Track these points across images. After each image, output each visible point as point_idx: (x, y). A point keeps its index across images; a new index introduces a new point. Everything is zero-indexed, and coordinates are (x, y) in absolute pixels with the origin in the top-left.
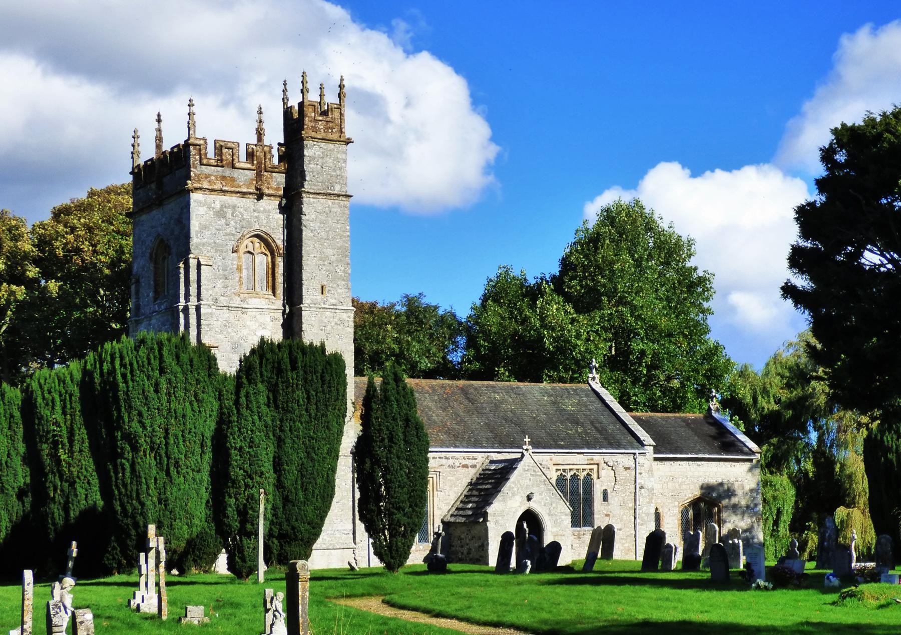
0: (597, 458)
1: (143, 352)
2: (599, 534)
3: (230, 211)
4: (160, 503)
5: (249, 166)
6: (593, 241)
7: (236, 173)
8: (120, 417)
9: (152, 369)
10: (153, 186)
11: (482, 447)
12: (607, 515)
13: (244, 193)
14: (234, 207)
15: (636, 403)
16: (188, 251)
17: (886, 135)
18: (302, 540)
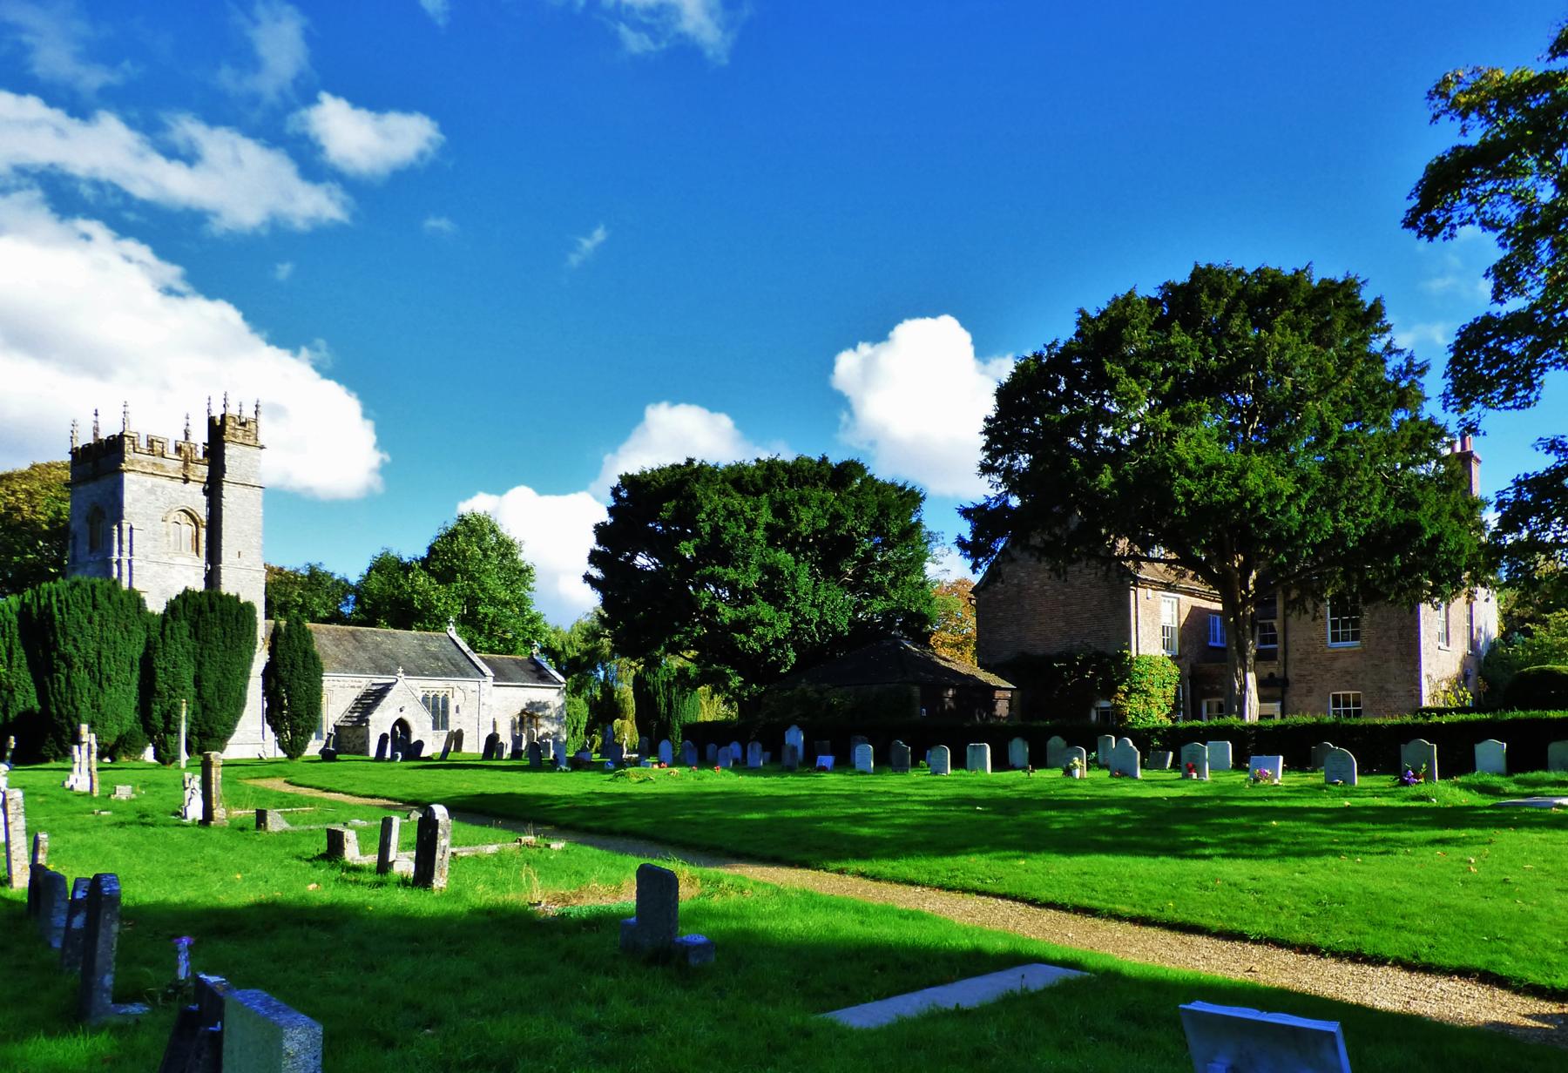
0: (452, 684)
1: (77, 592)
6: (453, 535)
8: (56, 642)
16: (121, 517)
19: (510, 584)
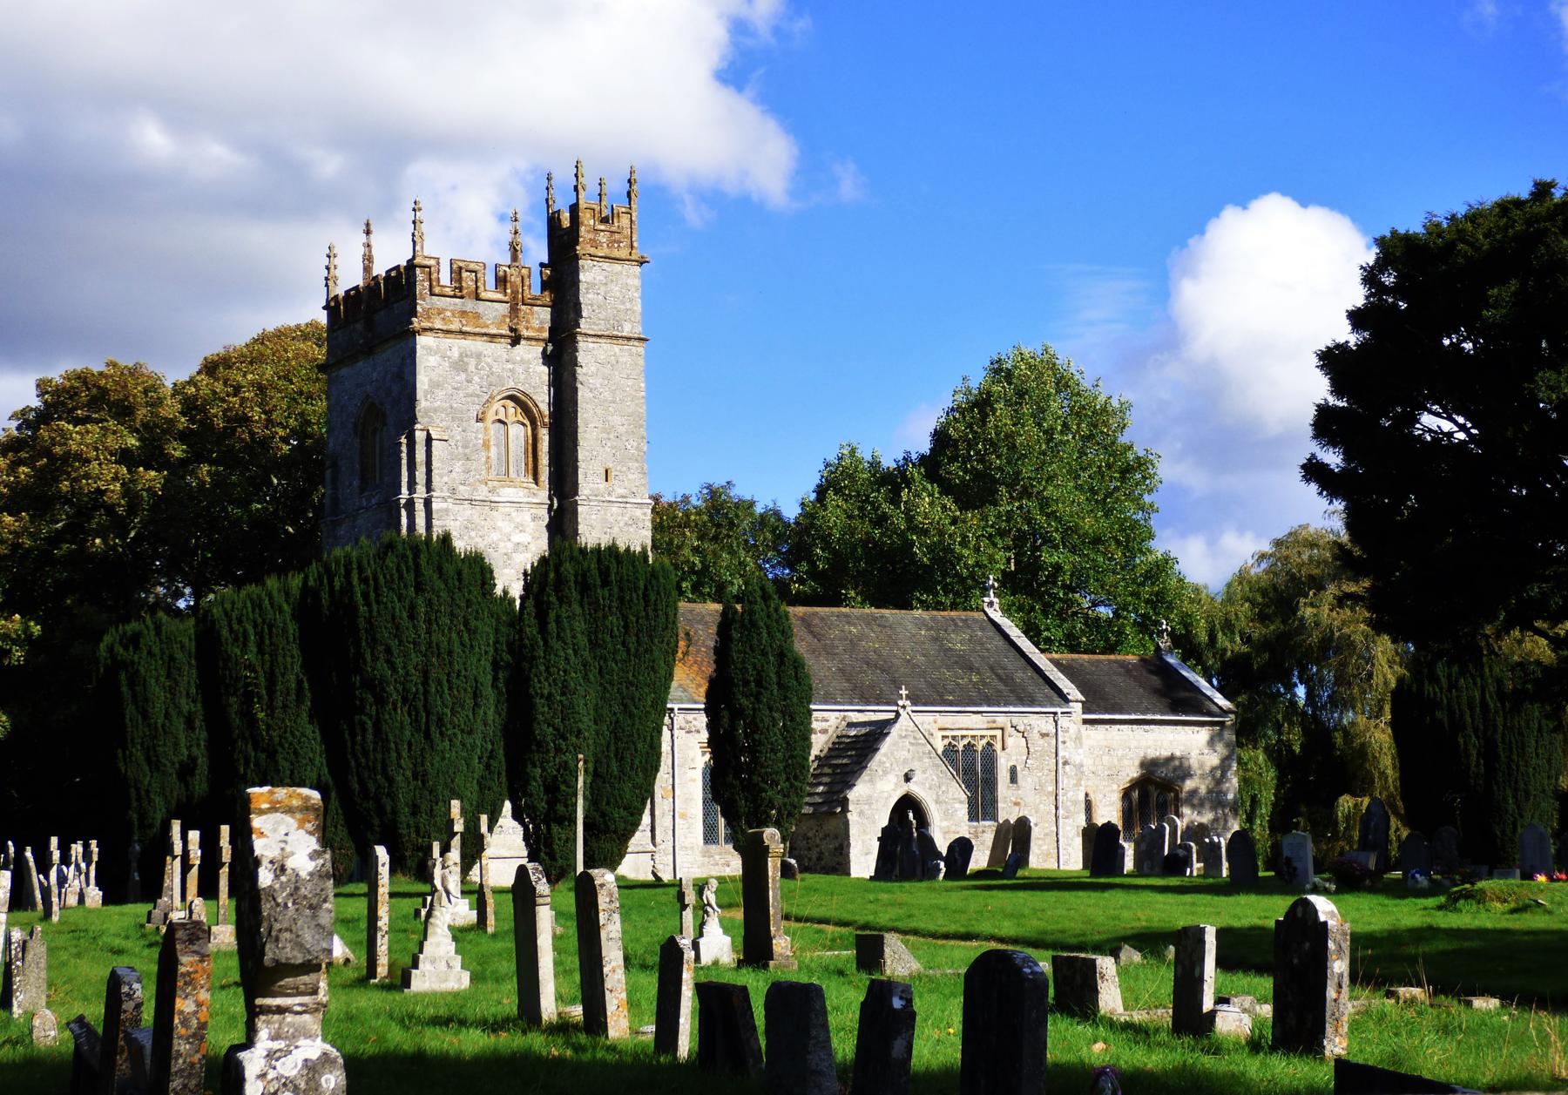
0: (1001, 720)
1: (391, 561)
2: (1007, 831)
3: (472, 362)
4: (415, 777)
5: (500, 296)
6: (982, 404)
7: (481, 307)
8: (360, 655)
9: (406, 586)
10: (359, 326)
11: (836, 703)
12: (1016, 804)
13: (494, 336)
14: (479, 356)
15: (1048, 641)
16: (413, 420)
17: (1461, 246)
18: (615, 832)
19: (1103, 502)
